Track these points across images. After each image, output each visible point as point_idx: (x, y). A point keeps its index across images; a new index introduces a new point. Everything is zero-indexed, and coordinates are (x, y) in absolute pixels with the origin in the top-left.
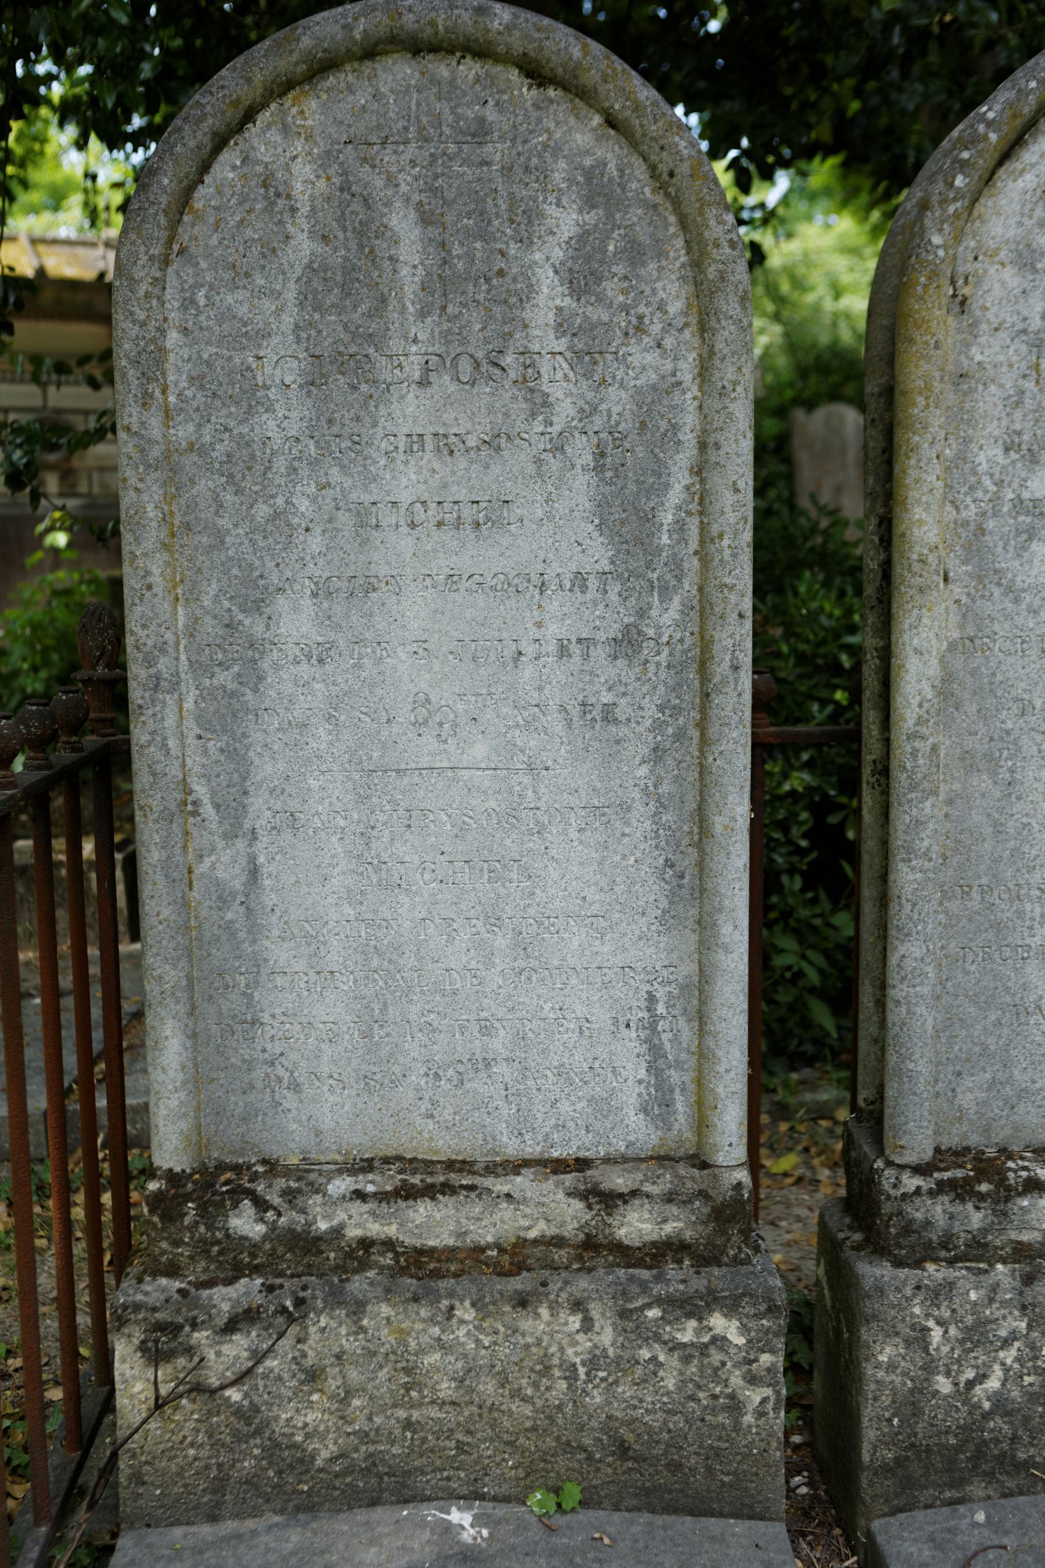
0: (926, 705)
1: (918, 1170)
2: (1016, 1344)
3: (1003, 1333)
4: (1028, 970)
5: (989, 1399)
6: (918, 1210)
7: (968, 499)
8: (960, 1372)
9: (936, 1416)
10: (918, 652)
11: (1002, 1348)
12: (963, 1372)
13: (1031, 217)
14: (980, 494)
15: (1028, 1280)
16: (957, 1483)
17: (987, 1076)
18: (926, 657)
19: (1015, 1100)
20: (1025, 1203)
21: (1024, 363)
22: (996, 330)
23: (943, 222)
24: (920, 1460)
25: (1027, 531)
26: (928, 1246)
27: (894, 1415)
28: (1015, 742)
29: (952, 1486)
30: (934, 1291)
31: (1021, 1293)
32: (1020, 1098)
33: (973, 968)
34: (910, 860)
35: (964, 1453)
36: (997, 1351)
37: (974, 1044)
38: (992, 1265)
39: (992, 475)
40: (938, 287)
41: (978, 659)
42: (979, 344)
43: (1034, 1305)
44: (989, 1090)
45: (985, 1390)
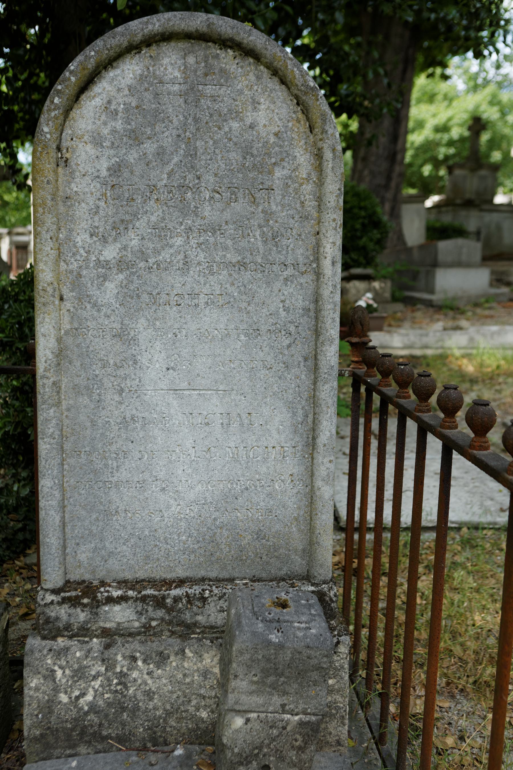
0: (49, 362)
1: (55, 592)
2: (100, 678)
3: (93, 673)
4: (111, 493)
5: (87, 705)
6: (52, 612)
7: (72, 260)
8: (72, 692)
9: (60, 713)
10: (44, 336)
11: (92, 680)
12: (73, 692)
13: (99, 120)
14: (78, 257)
15: (107, 647)
16: (73, 746)
17: (93, 545)
18: (48, 338)
19: (107, 557)
20: (107, 609)
21: (98, 192)
22: (84, 175)
23: (48, 121)
24: (53, 735)
25: (103, 276)
26: (58, 629)
27: (39, 713)
28: (100, 381)
29: (70, 747)
30: (58, 652)
31: (102, 653)
32: (109, 556)
33: (83, 492)
34: (43, 439)
35: (76, 731)
36: (90, 682)
37: (85, 529)
38: (91, 639)
39: (84, 248)
40: (47, 153)
41: (80, 339)
42: (76, 183)
43: (109, 660)
44: (94, 552)
45: (85, 701)
